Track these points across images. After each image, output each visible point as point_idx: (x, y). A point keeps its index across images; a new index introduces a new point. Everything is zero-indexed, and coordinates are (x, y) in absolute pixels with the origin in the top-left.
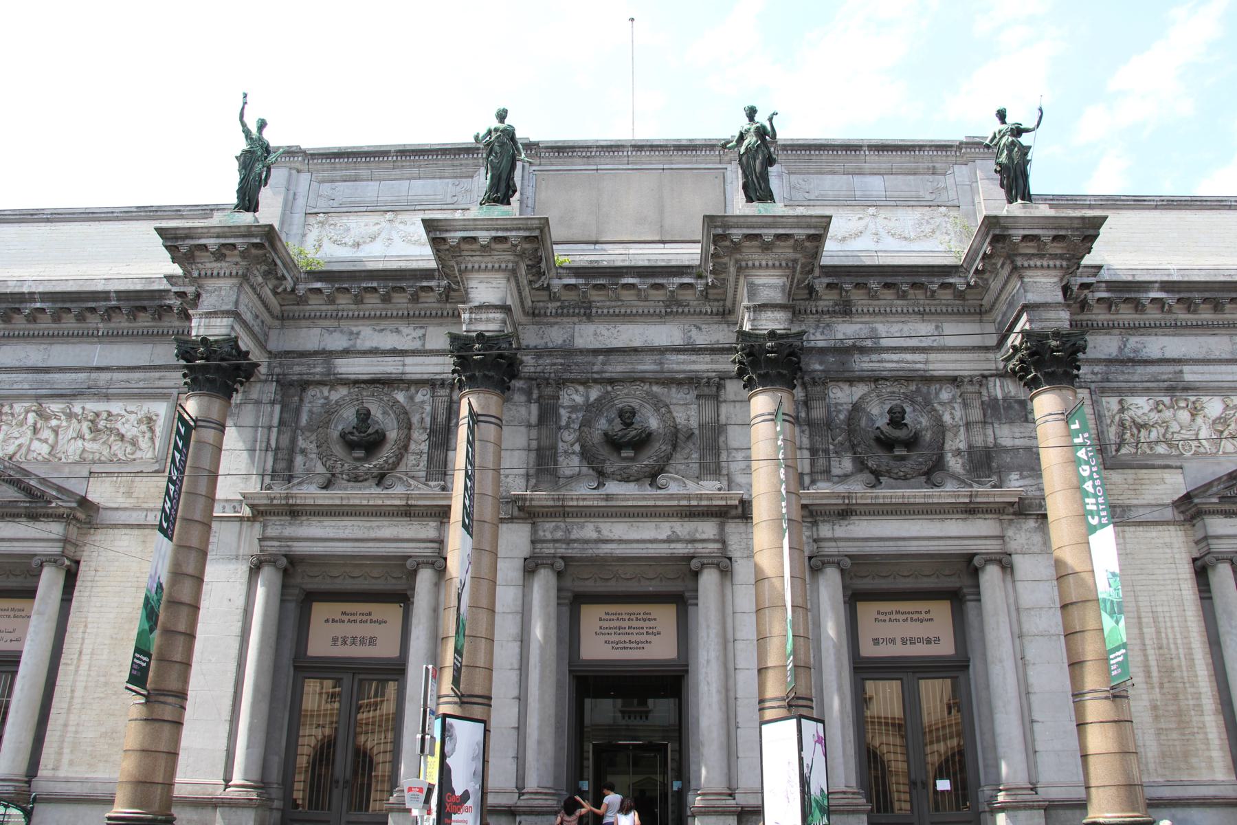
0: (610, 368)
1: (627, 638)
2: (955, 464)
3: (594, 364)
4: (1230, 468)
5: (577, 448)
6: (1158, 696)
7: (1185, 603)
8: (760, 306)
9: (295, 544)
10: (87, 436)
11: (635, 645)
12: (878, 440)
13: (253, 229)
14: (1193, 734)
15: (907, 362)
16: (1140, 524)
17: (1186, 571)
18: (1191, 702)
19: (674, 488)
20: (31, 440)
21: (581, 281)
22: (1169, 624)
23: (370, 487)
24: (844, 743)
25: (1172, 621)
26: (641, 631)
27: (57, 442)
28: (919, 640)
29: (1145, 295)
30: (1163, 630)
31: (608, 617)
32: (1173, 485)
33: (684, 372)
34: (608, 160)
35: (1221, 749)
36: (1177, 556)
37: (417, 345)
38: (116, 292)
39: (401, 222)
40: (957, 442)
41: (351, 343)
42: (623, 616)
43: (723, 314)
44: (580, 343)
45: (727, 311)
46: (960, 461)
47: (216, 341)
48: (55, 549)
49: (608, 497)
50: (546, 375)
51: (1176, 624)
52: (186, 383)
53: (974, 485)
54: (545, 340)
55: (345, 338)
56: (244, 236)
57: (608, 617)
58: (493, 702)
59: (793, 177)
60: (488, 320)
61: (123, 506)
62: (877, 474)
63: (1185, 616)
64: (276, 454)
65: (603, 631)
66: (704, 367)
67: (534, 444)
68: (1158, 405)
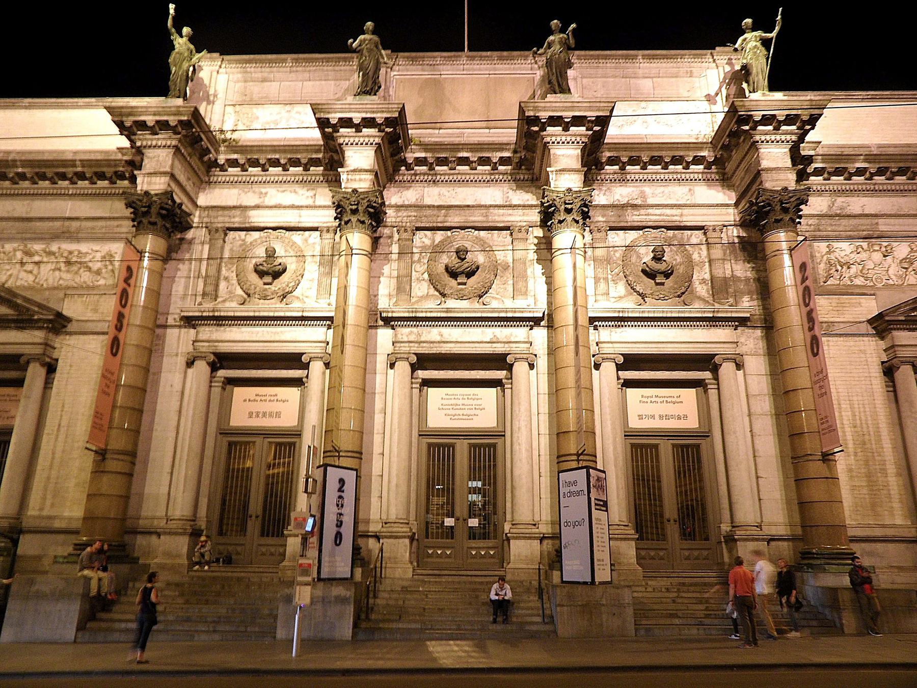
0: (450, 219)
1: (461, 412)
2: (702, 290)
3: (438, 216)
4: (911, 295)
5: (426, 276)
6: (853, 462)
7: (875, 394)
8: (560, 170)
9: (220, 344)
10: (63, 268)
11: (467, 417)
12: (643, 271)
13: (181, 109)
14: (879, 490)
15: (667, 215)
16: (841, 335)
17: (876, 372)
18: (877, 467)
19: (495, 304)
20: (19, 271)
21: (429, 155)
22: (862, 410)
23: (276, 304)
24: (618, 488)
25: (864, 407)
26: (471, 407)
27: (39, 273)
28: (672, 417)
29: (851, 165)
30: (857, 414)
31: (448, 397)
32: (870, 307)
33: (504, 222)
34: (449, 67)
35: (901, 502)
36: (869, 359)
37: (310, 202)
38: (80, 160)
39: (297, 112)
40: (702, 274)
41: (261, 200)
42: (458, 397)
43: (532, 180)
44: (428, 201)
45: (535, 178)
46: (705, 288)
47: (156, 195)
48: (38, 350)
49: (448, 310)
50: (404, 224)
51: (867, 409)
52: (134, 226)
53: (716, 304)
54: (402, 199)
55: (257, 196)
56: (175, 115)
57: (448, 397)
58: (363, 457)
59: (585, 80)
60: (360, 180)
61: (91, 319)
62: (643, 296)
63: (875, 404)
64: (205, 281)
65: (444, 407)
66: (518, 218)
67: (395, 273)
68: (857, 248)
